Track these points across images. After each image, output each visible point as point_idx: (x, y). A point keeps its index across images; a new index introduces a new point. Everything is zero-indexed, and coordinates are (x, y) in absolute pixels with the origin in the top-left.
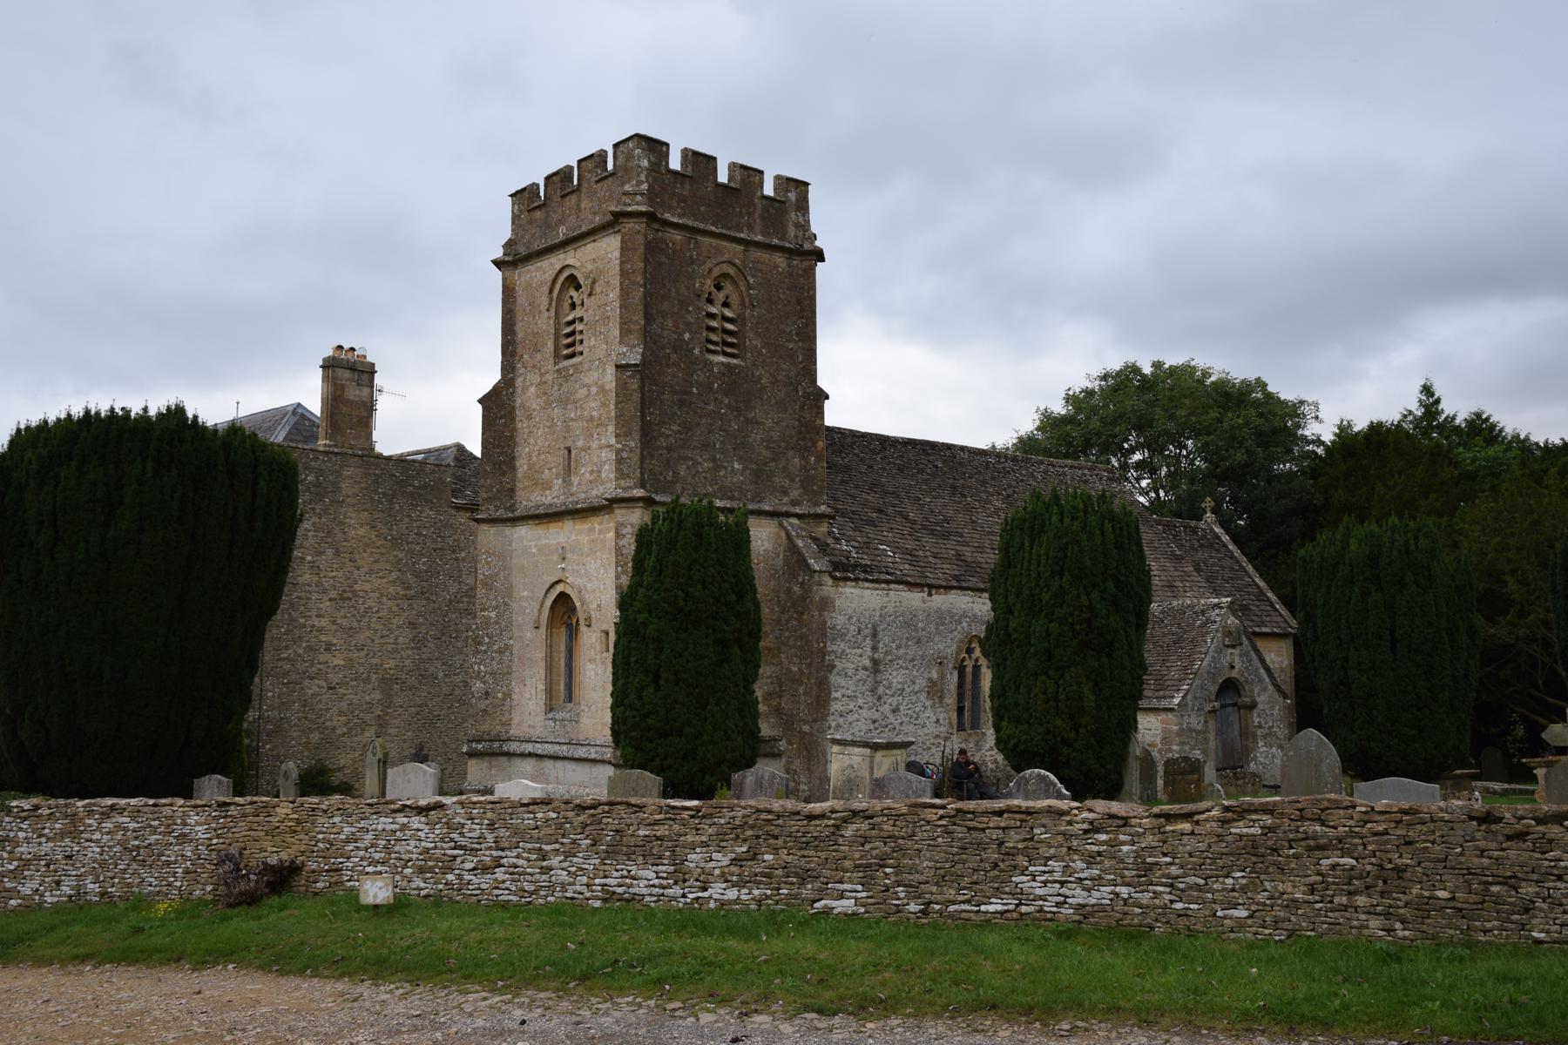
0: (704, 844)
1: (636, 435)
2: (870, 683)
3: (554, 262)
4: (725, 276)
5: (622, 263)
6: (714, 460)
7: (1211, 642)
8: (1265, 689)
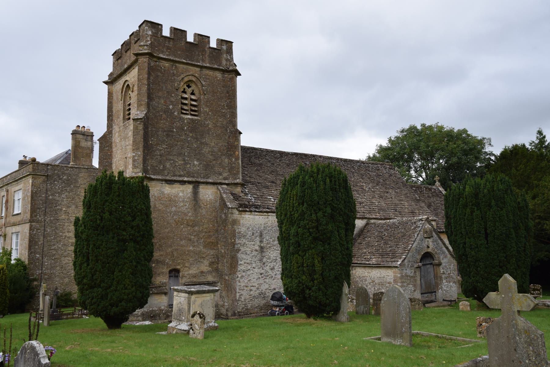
1: (141, 149)
2: (259, 257)
4: (191, 81)
6: (184, 160)
7: (418, 237)
8: (446, 257)
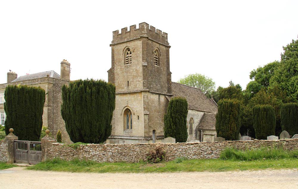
0: (256, 147)
3: (124, 46)
5: (142, 46)
